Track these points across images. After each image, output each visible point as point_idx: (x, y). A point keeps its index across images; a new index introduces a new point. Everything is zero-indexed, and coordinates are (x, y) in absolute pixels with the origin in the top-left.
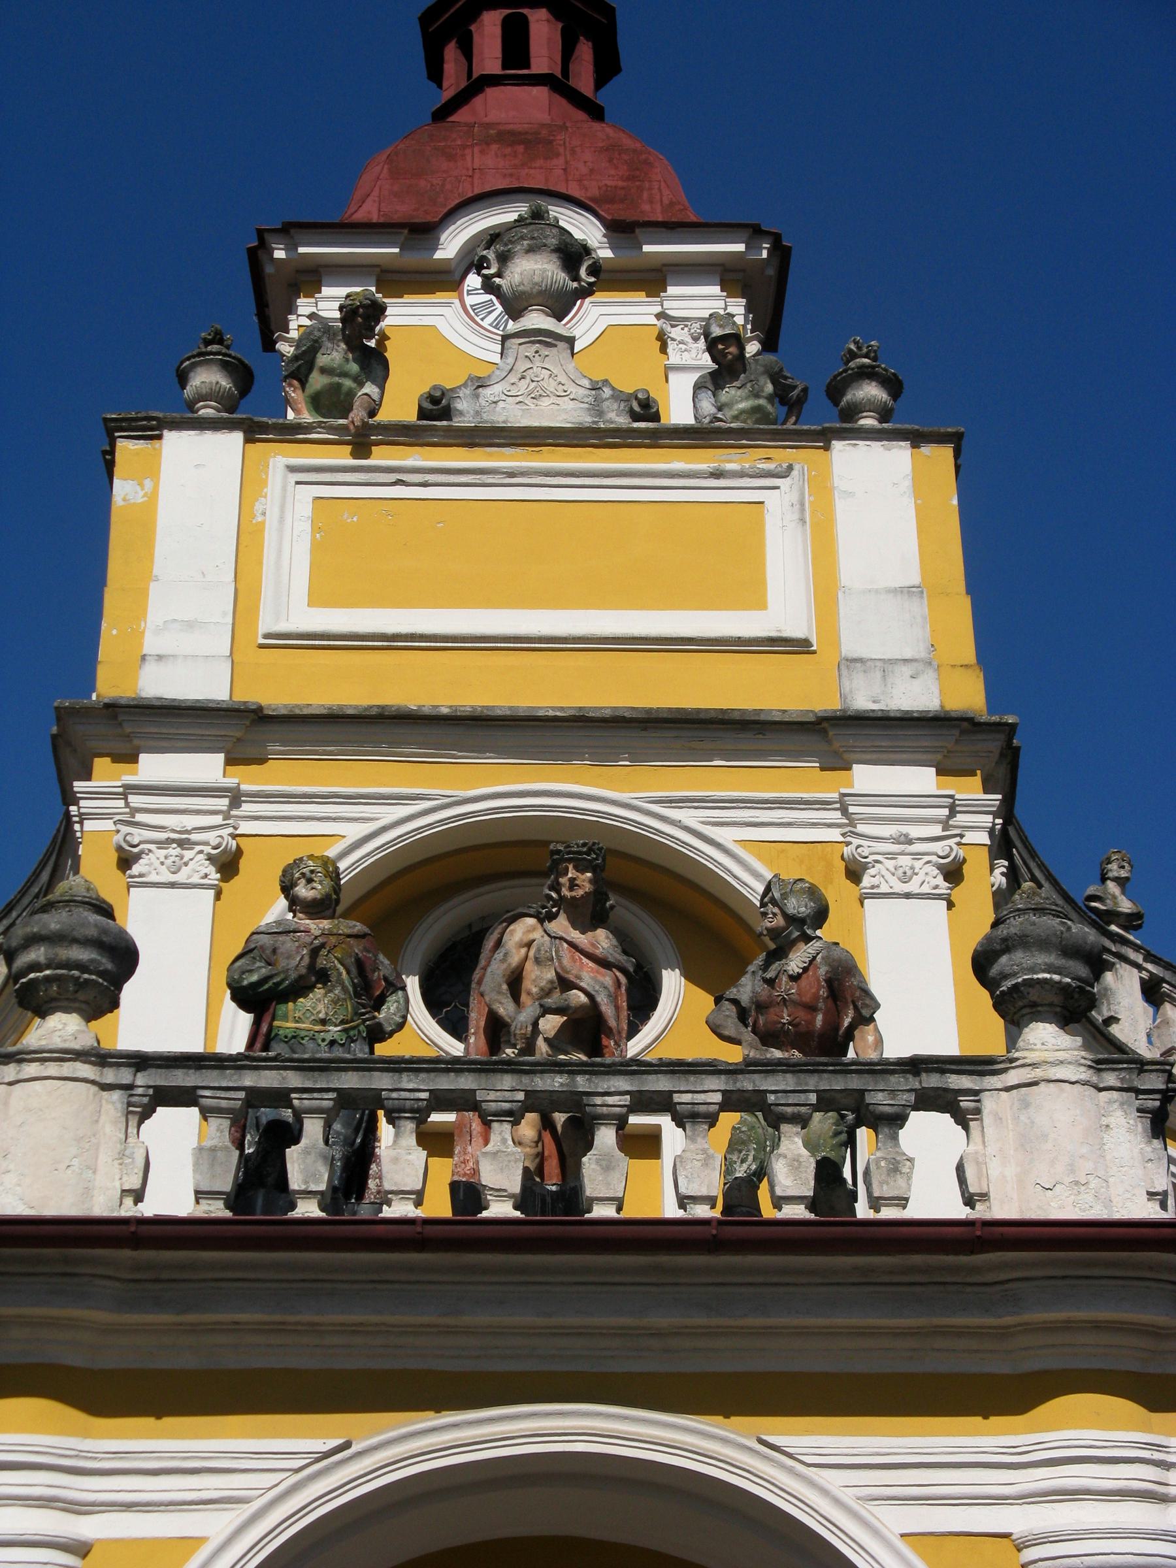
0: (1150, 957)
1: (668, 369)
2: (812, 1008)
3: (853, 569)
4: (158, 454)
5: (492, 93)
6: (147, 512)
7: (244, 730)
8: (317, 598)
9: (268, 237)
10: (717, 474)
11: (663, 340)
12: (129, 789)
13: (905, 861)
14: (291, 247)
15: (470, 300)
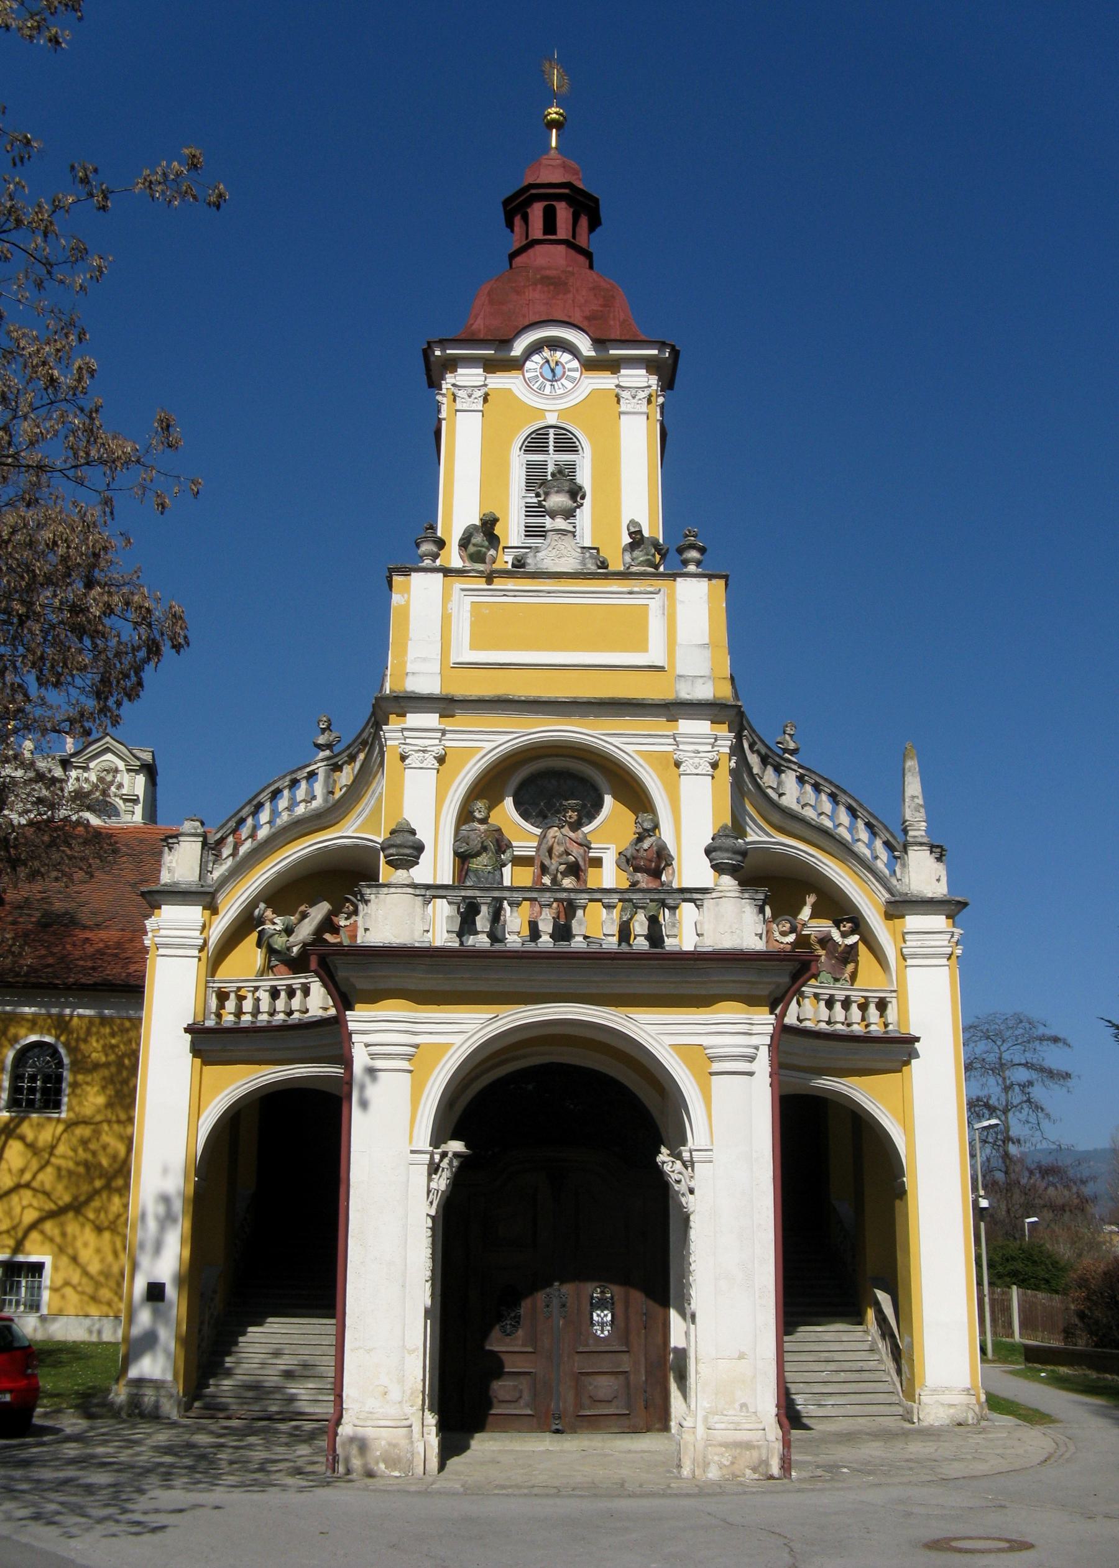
0: (801, 767)
1: (620, 413)
2: (651, 861)
3: (682, 636)
4: (409, 582)
5: (538, 248)
6: (405, 609)
7: (446, 705)
8: (474, 646)
9: (433, 345)
10: (630, 593)
11: (618, 398)
12: (403, 730)
13: (697, 760)
14: (443, 350)
15: (527, 375)
